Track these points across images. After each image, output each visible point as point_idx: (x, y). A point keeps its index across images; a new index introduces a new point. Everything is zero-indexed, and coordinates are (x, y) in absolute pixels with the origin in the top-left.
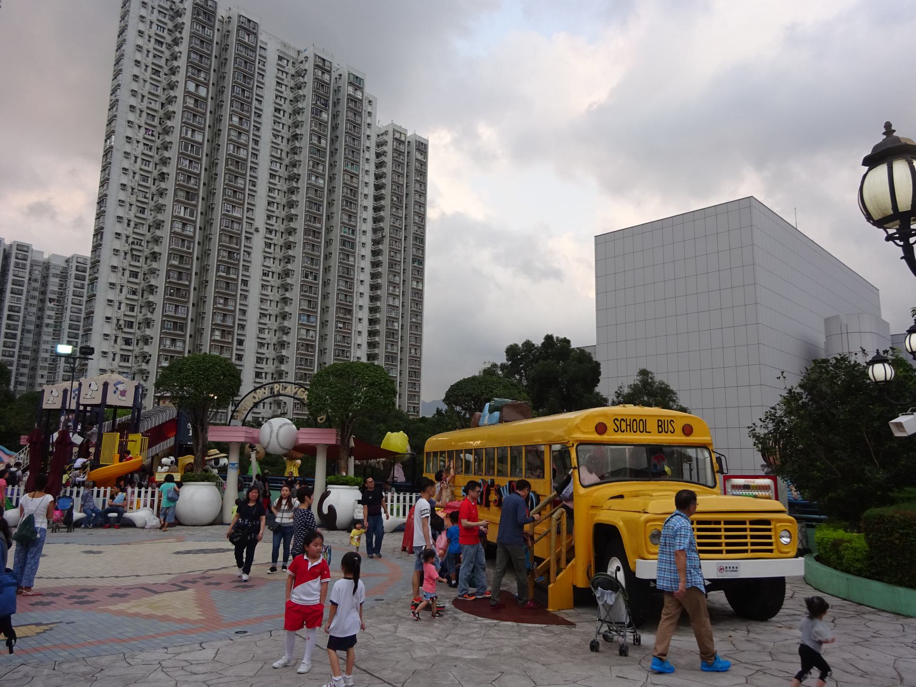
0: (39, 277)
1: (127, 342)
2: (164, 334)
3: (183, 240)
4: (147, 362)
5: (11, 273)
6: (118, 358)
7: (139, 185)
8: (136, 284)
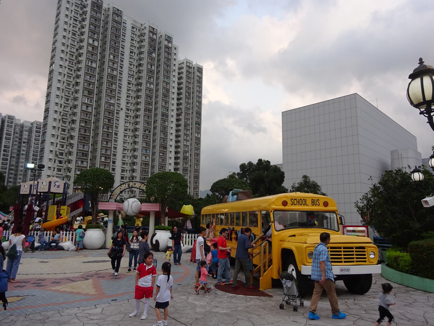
0: (19, 131)
1: (60, 162)
2: (78, 159)
3: (87, 114)
4: (70, 172)
5: (5, 129)
6: (56, 170)
7: (66, 88)
8: (65, 135)
